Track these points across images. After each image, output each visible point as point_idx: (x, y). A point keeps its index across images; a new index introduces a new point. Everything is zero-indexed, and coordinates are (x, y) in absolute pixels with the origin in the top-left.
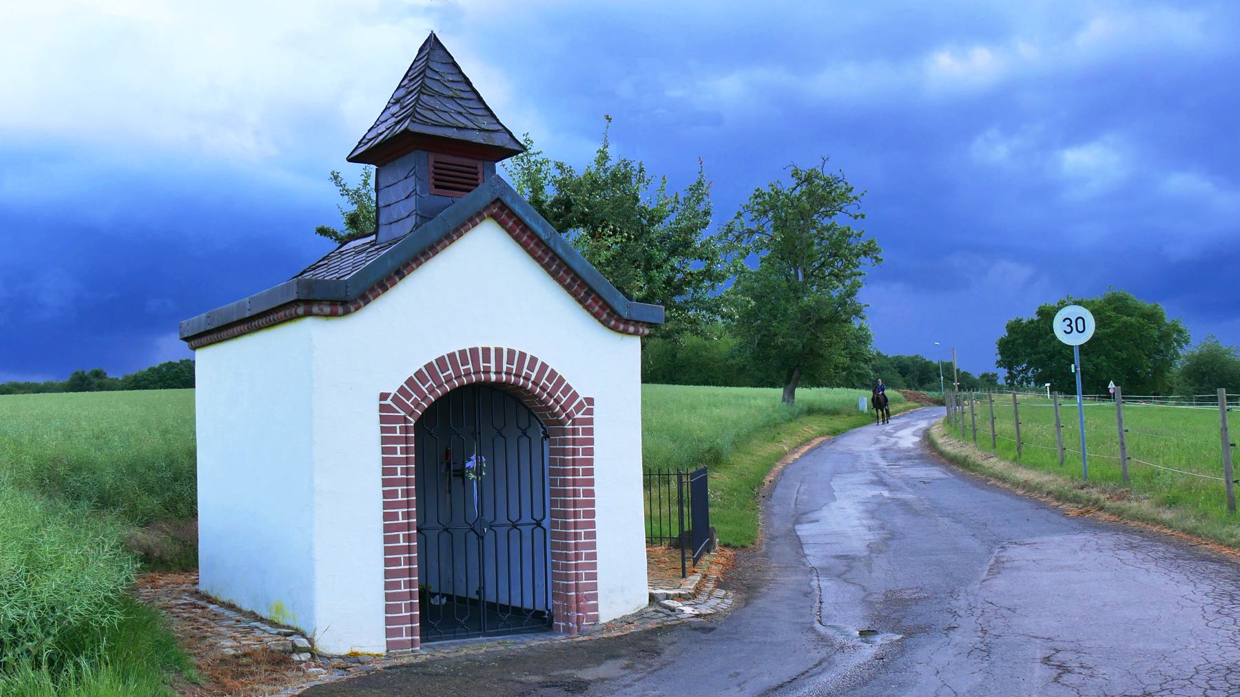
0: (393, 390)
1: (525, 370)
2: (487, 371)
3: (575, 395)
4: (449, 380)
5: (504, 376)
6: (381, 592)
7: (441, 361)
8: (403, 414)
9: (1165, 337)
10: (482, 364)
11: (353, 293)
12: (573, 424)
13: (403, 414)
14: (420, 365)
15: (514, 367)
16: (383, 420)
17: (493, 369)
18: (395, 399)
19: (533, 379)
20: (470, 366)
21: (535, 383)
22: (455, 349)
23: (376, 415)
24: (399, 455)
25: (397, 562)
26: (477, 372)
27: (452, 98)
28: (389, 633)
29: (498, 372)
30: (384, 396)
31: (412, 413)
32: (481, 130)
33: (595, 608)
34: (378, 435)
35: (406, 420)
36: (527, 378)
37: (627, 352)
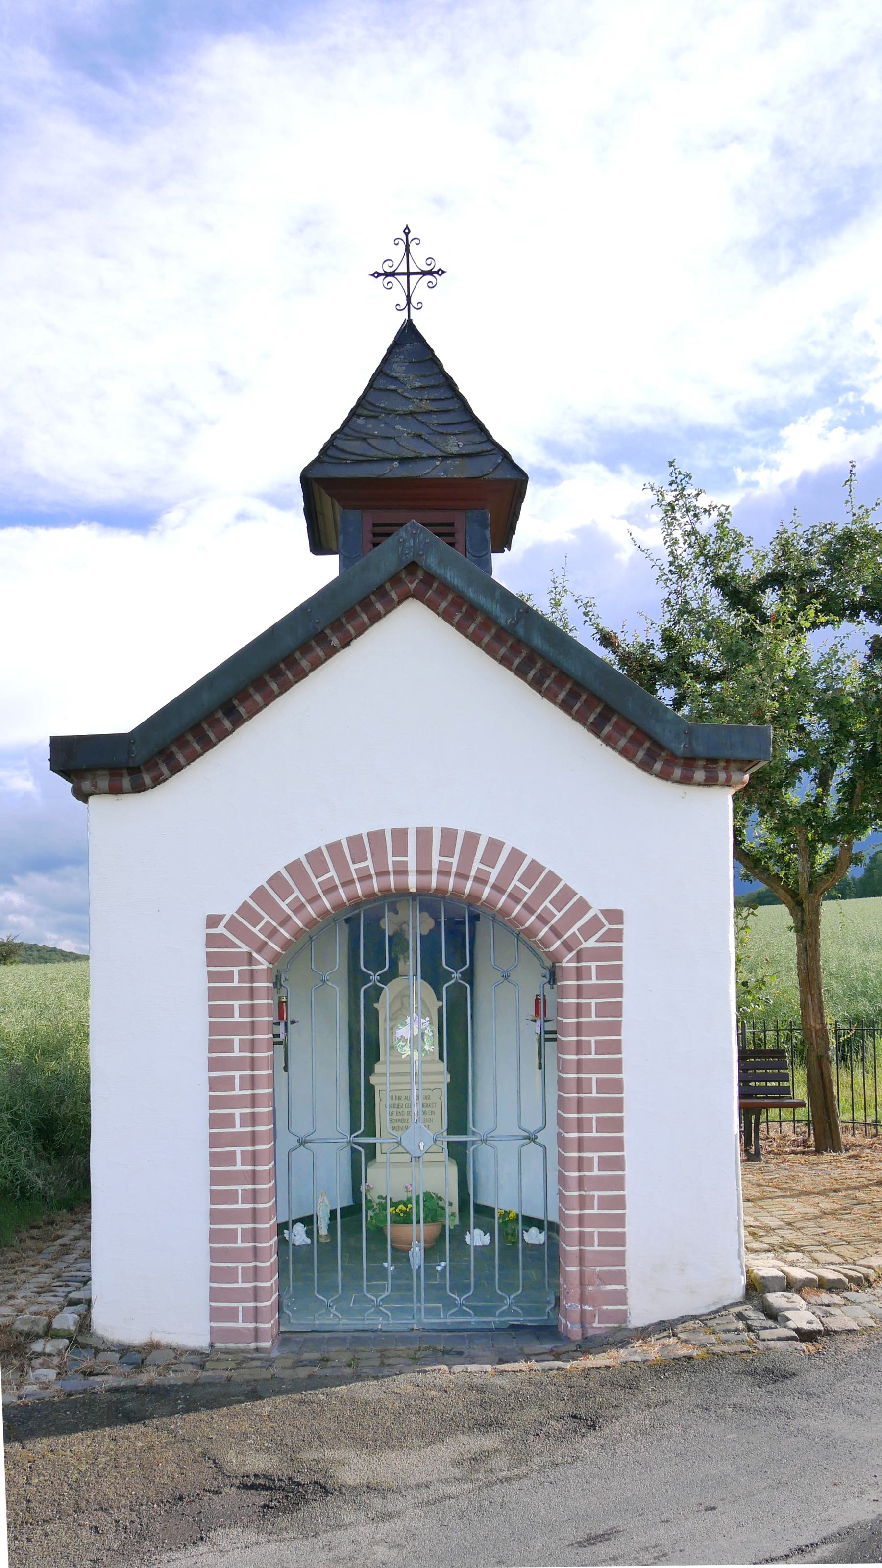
0: (229, 909)
1: (476, 865)
2: (401, 871)
3: (583, 906)
4: (330, 889)
5: (342, 893)
6: (202, 1247)
7: (315, 857)
8: (245, 949)
9: (86, 785)
10: (391, 859)
11: (139, 754)
12: (579, 958)
13: (245, 949)
14: (278, 865)
15: (455, 861)
16: (211, 959)
17: (412, 867)
18: (232, 925)
19: (492, 880)
20: (369, 863)
21: (498, 888)
22: (341, 835)
23: (200, 951)
24: (237, 1018)
25: (231, 1197)
26: (383, 873)
27: (411, 413)
28: (215, 1314)
29: (423, 872)
30: (213, 921)
31: (262, 947)
32: (447, 457)
33: (621, 1298)
34: (202, 984)
35: (251, 960)
36: (481, 880)
37: (705, 819)
